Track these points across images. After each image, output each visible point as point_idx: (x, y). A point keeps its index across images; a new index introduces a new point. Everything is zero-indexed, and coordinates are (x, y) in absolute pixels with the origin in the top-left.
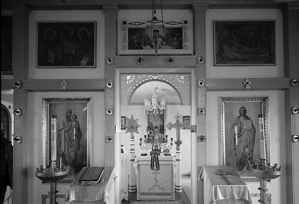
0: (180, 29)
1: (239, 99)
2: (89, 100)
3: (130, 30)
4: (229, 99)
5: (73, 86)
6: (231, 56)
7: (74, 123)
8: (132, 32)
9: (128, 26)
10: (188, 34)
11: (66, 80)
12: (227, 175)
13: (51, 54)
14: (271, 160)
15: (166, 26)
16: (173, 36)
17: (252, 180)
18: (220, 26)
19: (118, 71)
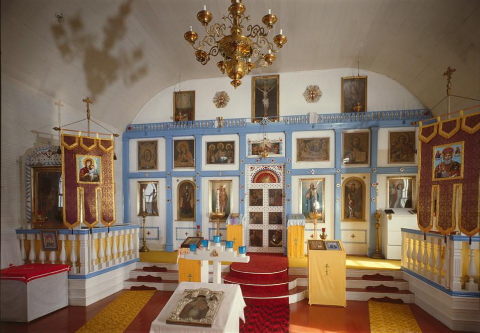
0: (279, 143)
1: (310, 179)
2: (231, 181)
3: (252, 144)
4: (305, 179)
5: (224, 173)
6: (306, 157)
7: (224, 193)
8: (254, 145)
9: (252, 143)
10: (283, 146)
11: (314, 169)
12: (331, 278)
13: (213, 158)
14: (326, 211)
15: (271, 142)
16: (275, 147)
17: (330, 242)
18: (300, 141)
19: (246, 165)
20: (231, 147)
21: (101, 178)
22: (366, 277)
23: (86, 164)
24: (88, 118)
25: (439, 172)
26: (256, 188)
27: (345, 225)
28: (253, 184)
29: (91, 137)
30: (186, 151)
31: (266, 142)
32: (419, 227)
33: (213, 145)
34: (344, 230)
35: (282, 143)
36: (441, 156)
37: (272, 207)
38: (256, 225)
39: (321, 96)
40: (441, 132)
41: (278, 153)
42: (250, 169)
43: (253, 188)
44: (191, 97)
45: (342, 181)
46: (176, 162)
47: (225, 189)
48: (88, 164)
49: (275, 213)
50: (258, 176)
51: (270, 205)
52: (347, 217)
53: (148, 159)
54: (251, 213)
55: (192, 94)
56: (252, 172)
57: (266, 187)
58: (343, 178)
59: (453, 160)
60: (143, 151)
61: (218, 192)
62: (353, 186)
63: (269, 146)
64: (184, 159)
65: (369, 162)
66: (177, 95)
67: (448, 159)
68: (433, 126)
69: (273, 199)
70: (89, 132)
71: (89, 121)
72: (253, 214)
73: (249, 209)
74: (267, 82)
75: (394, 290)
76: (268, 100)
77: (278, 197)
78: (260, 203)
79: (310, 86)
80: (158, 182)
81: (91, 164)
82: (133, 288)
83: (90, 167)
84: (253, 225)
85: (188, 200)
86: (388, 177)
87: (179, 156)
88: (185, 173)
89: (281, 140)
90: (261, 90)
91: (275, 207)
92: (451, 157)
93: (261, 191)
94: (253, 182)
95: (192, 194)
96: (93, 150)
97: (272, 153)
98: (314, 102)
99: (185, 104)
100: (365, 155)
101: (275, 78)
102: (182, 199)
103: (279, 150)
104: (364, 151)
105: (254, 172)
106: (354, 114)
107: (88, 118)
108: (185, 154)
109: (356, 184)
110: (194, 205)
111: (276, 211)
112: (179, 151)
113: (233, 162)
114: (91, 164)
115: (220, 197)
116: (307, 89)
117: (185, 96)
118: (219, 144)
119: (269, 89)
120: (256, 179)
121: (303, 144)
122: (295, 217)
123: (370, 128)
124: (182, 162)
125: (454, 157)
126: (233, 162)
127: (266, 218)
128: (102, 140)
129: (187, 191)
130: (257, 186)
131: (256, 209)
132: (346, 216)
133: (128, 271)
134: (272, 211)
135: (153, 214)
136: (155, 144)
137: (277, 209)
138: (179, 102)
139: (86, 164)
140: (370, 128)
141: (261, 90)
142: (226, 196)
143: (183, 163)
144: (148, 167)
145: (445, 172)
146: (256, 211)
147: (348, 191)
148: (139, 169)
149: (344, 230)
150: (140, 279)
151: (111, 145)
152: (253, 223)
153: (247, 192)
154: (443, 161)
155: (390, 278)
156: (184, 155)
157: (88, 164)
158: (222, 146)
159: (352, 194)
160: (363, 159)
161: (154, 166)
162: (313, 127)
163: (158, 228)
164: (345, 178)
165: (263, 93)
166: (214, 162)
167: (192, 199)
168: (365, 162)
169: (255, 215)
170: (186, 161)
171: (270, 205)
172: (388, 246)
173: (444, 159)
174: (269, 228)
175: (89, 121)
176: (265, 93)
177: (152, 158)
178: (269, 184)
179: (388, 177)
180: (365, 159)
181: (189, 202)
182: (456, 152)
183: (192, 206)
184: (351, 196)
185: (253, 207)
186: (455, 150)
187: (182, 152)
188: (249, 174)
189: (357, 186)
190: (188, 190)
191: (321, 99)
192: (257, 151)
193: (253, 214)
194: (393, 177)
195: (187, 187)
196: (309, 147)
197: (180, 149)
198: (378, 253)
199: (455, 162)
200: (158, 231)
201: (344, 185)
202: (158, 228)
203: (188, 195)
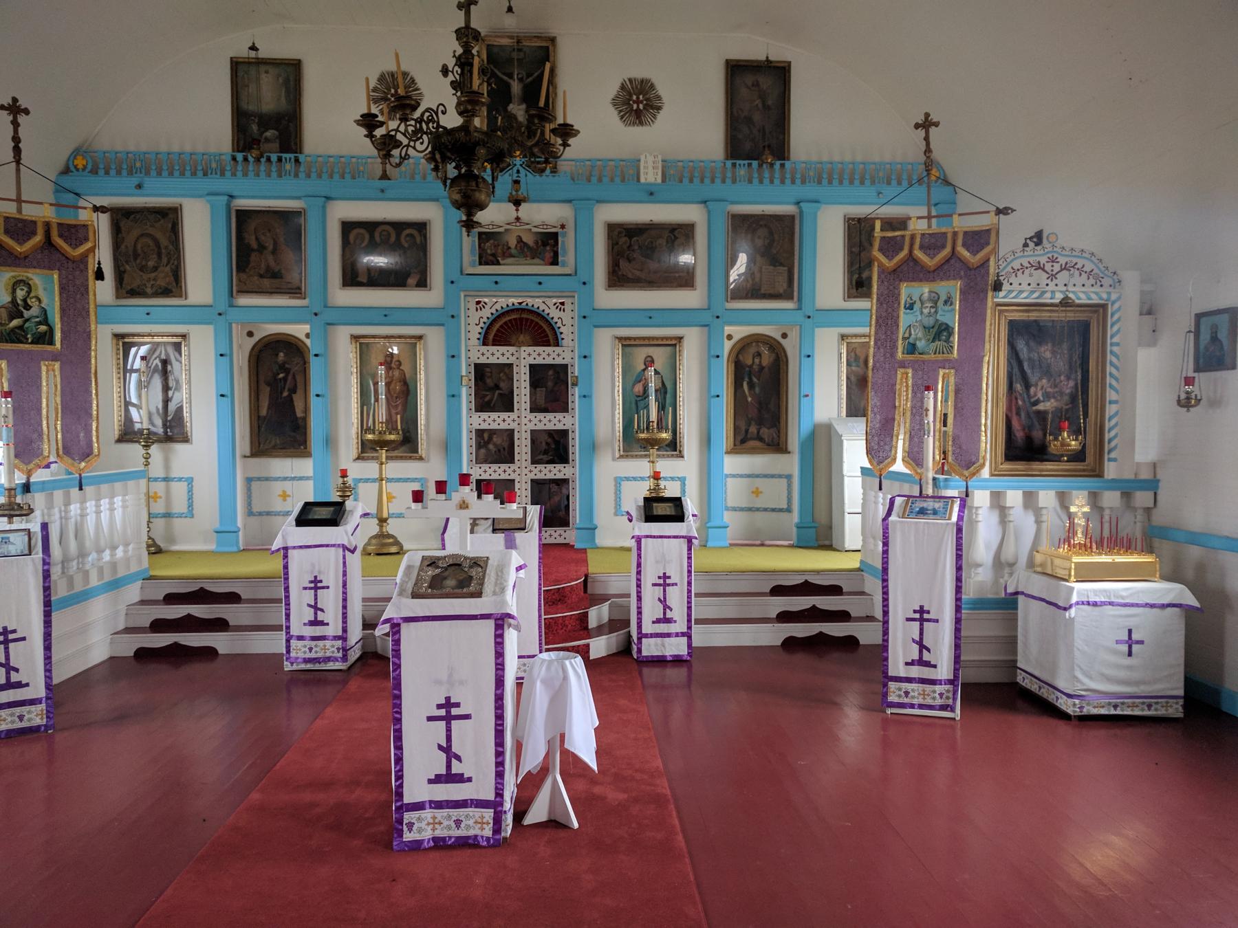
0: (556, 234)
6: (630, 276)
7: (397, 373)
16: (545, 244)
20: (418, 240)
21: (58, 336)
22: (778, 591)
23: (14, 291)
24: (18, 161)
25: (911, 340)
26: (493, 360)
27: (733, 464)
28: (484, 349)
29: (29, 212)
30: (275, 243)
31: (517, 230)
32: (870, 462)
33: (362, 231)
34: (734, 476)
35: (565, 235)
36: (917, 306)
37: (540, 416)
38: (495, 467)
39: (659, 108)
40: (918, 253)
41: (555, 262)
42: (473, 306)
43: (483, 360)
44: (287, 81)
45: (728, 345)
46: (243, 276)
47: (400, 364)
48: (20, 294)
49: (550, 433)
50: (497, 326)
51: (535, 409)
52: (742, 441)
53: (151, 264)
54: (480, 433)
55: (291, 71)
56: (480, 313)
57: (523, 358)
58: (730, 337)
59: (938, 317)
60: (129, 240)
61: (381, 371)
62: (757, 361)
63: (529, 239)
64: (268, 268)
65: (796, 294)
66: (242, 71)
67: (930, 315)
68: (903, 236)
69: (541, 392)
70: (19, 201)
71: (18, 170)
72: (486, 436)
73: (472, 421)
74: (522, 55)
75: (843, 616)
76: (524, 106)
77: (552, 387)
78: (507, 404)
79: (630, 80)
80: (184, 336)
81: (29, 292)
82: (143, 655)
83: (25, 300)
84: (485, 466)
85: (285, 394)
86: (843, 337)
87: (254, 257)
88: (275, 316)
89: (563, 227)
90: (505, 78)
91: (550, 416)
92: (936, 312)
93: (506, 370)
94: (484, 344)
95: (299, 379)
96: (35, 250)
97: (536, 261)
98: (641, 123)
99: (268, 97)
100: (786, 275)
101: (544, 44)
102: (266, 391)
103: (556, 254)
104: (782, 265)
105: (486, 313)
106: (755, 163)
107: (18, 161)
108: (274, 252)
109: (765, 351)
110: (306, 410)
111: (550, 427)
112: (254, 245)
113: (423, 283)
114: (29, 292)
115: (388, 385)
116: (623, 87)
117: (267, 72)
118: (379, 229)
119: (528, 76)
120: (491, 337)
121: (624, 239)
122: (180, 516)
123: (798, 203)
124: (261, 276)
125: (940, 312)
126: (423, 283)
127: (523, 448)
128: (59, 224)
129: (282, 368)
130: (497, 355)
131: (495, 421)
132: (739, 438)
133: (122, 608)
134: (540, 427)
135: (168, 439)
136: (170, 218)
137: (551, 421)
138: (252, 88)
139: (14, 291)
140: (798, 203)
141: (505, 78)
142: (405, 383)
143: (266, 282)
144: (149, 290)
145: (923, 342)
146: (494, 426)
147: (740, 372)
148: (117, 297)
149: (734, 476)
150: (159, 626)
151: (86, 239)
152: (485, 462)
153: (465, 369)
154: (919, 318)
155: (835, 590)
156: (271, 258)
157: (20, 294)
158: (389, 234)
159: (755, 380)
160: (781, 287)
161: (173, 286)
162: (651, 195)
163: (190, 481)
164: (736, 338)
165: (508, 86)
166: (365, 281)
167: (300, 391)
168: (788, 296)
169: (490, 439)
170: (276, 275)
171: (535, 409)
172: (847, 516)
173: (922, 313)
174: (532, 476)
175: (18, 170)
176: (516, 88)
177: (165, 260)
178: (530, 349)
179: (843, 337)
180: (785, 285)
181: (290, 400)
182: (946, 302)
183: (299, 414)
184: (751, 386)
185: (485, 415)
186: (943, 298)
187: (262, 248)
188: (473, 322)
189: (767, 358)
190: (284, 363)
191: (661, 116)
192: (494, 255)
193: (486, 436)
194: (856, 336)
195: (281, 354)
196: (640, 247)
197: (257, 239)
198: (821, 534)
199: (942, 324)
200: (190, 491)
201: (733, 355)
202: (190, 481)
203: (285, 379)
